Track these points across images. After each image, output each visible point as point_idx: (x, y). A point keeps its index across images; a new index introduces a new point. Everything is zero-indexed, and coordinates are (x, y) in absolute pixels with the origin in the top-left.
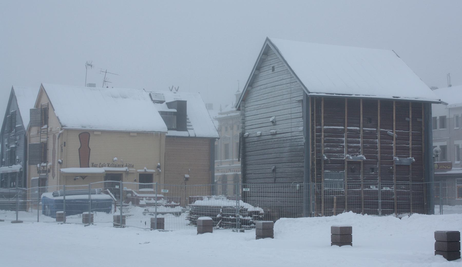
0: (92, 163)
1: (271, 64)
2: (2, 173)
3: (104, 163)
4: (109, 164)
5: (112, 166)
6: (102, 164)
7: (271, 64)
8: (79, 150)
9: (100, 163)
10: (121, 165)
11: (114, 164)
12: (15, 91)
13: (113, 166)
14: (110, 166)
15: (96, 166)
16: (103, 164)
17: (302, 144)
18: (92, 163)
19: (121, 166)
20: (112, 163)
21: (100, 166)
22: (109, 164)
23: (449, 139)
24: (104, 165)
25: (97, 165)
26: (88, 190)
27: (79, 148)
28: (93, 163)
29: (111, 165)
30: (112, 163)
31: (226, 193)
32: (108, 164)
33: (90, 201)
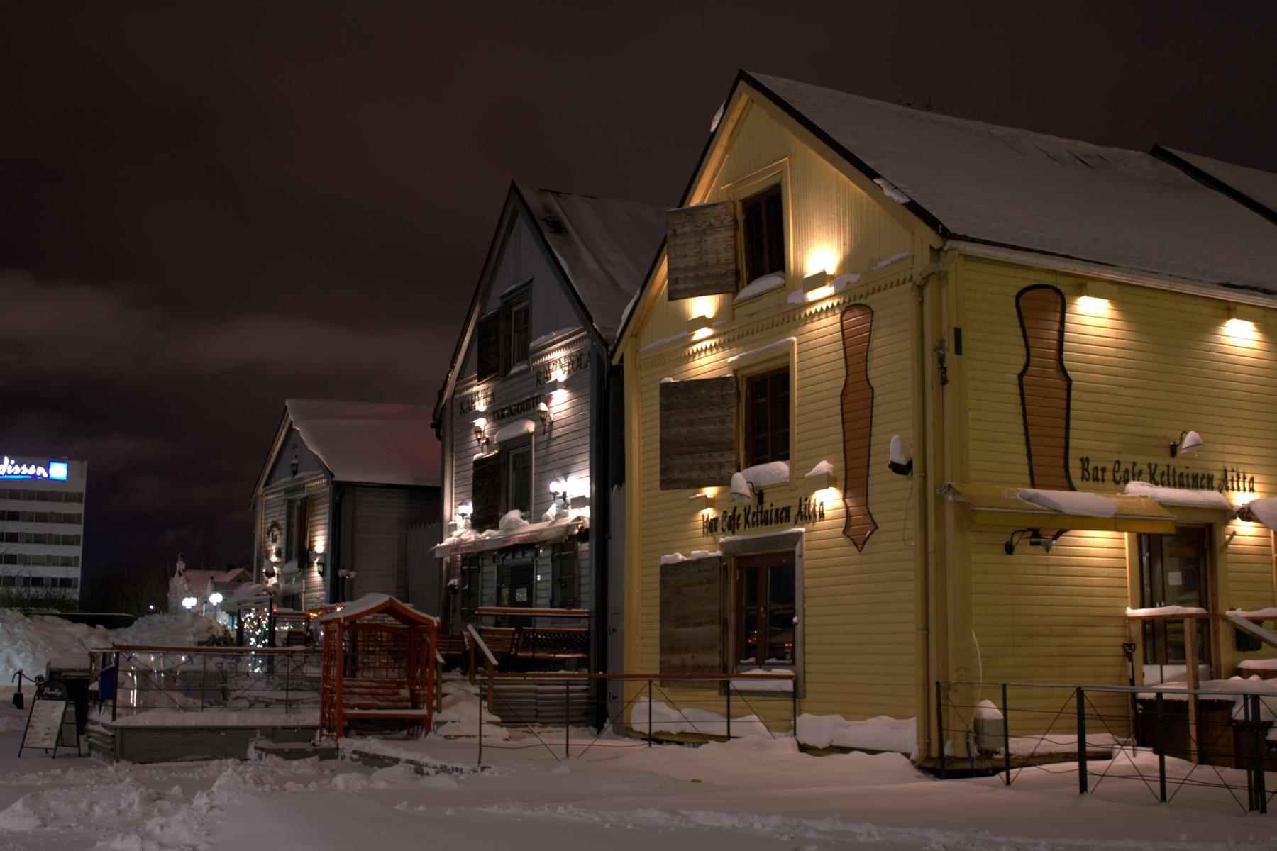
0: (1082, 459)
1: (1131, 406)
2: (85, 478)
3: (1134, 464)
4: (1153, 467)
5: (1165, 478)
6: (1123, 468)
7: (1131, 406)
8: (1021, 385)
9: (1118, 462)
10: (1203, 476)
11: (1174, 473)
12: (848, 163)
13: (1171, 482)
14: (1157, 478)
15: (1100, 477)
16: (1131, 470)
17: (739, 698)
18: (1082, 459)
19: (1205, 481)
20: (1168, 466)
21: (1118, 479)
22: (1153, 467)
23: (783, 694)
24: (1133, 472)
25: (1104, 470)
26: (1066, 757)
27: (1019, 372)
28: (1087, 460)
29: (1163, 474)
30: (1168, 466)
31: (350, 792)
32: (1150, 465)
33: (334, 708)
